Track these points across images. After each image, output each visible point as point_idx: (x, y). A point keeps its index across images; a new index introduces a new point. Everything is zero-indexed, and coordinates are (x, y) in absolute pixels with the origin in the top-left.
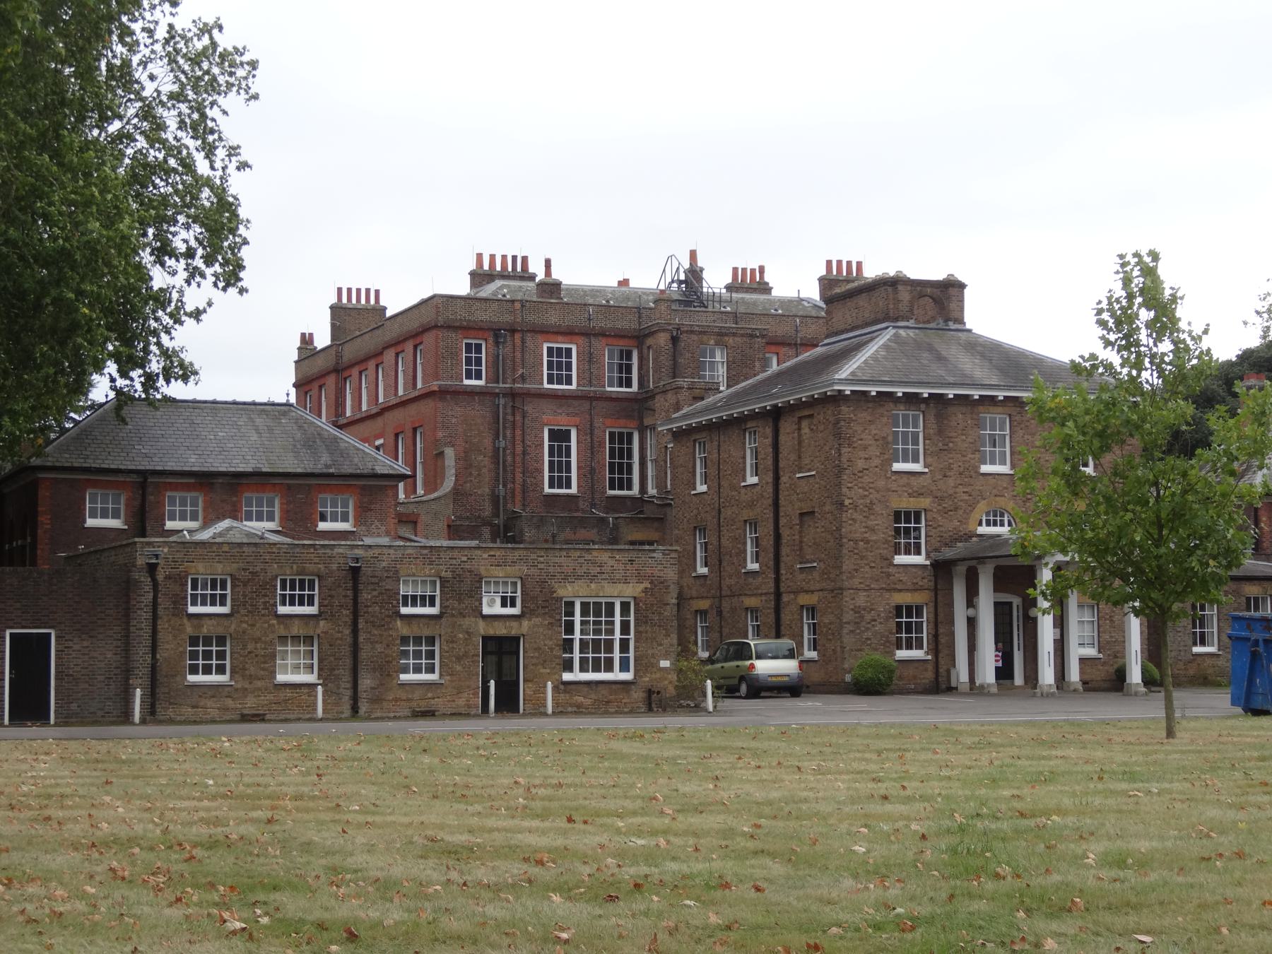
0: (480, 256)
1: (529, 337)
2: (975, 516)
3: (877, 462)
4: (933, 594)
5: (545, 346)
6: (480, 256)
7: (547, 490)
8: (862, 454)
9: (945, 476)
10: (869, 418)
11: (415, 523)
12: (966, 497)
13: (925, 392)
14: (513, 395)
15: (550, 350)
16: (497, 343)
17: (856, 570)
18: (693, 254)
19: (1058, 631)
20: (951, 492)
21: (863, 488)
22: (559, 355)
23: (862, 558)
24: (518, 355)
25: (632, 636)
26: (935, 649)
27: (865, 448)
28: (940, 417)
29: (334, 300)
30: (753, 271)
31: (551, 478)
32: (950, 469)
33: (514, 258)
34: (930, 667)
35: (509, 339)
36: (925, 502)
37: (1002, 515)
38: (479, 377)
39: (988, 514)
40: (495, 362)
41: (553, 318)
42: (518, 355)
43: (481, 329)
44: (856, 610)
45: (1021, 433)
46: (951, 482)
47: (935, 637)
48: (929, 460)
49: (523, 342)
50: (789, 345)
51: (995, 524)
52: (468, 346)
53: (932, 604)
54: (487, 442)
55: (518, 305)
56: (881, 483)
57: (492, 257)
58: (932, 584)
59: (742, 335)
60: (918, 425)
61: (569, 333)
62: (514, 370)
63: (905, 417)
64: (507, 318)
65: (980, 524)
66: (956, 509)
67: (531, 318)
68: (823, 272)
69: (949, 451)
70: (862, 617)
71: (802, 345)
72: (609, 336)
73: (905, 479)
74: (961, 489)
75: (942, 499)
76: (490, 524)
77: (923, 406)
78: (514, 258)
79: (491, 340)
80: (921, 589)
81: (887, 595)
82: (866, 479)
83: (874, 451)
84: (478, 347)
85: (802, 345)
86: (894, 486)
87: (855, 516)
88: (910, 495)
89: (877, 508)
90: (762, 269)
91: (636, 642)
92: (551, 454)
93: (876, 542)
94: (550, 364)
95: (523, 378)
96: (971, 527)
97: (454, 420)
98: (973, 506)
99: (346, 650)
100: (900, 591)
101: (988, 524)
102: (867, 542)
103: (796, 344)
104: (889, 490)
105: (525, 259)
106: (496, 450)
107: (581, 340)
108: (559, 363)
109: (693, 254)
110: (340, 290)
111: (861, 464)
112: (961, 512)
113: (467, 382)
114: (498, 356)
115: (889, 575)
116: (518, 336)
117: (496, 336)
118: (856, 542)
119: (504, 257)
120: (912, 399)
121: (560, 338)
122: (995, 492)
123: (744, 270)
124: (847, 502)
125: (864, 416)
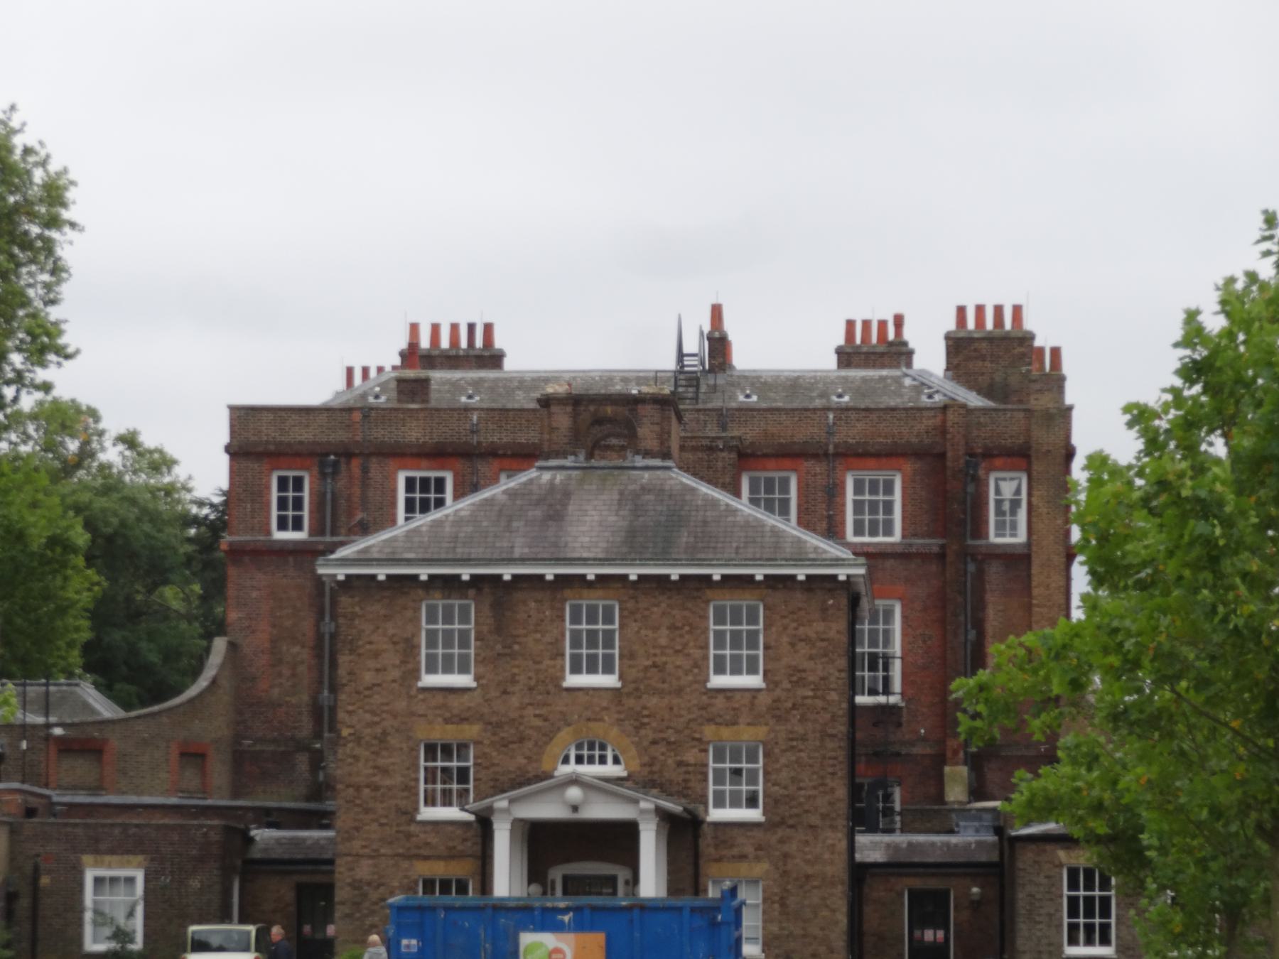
0: (414, 328)
1: (374, 464)
2: (555, 748)
3: (396, 674)
4: (479, 863)
6: (414, 328)
8: (371, 664)
9: (505, 692)
10: (383, 612)
12: (538, 722)
13: (466, 573)
15: (410, 483)
16: (323, 475)
17: (357, 829)
18: (717, 312)
20: (513, 715)
21: (373, 713)
23: (367, 811)
25: (1113, 921)
27: (377, 655)
28: (499, 608)
30: (882, 325)
32: (513, 680)
33: (471, 327)
35: (343, 467)
36: (472, 731)
37: (603, 747)
38: (298, 526)
39: (579, 747)
41: (414, 433)
42: (357, 491)
43: (298, 454)
44: (356, 885)
45: (634, 626)
46: (515, 701)
48: (482, 670)
49: (365, 471)
50: (815, 456)
51: (591, 760)
52: (283, 483)
53: (478, 878)
54: (307, 626)
55: (357, 416)
56: (401, 705)
57: (435, 329)
58: (478, 848)
59: (695, 449)
60: (467, 619)
62: (350, 514)
64: (341, 436)
65: (566, 760)
66: (522, 740)
67: (381, 434)
68: (951, 325)
69: (513, 656)
70: (365, 895)
71: (836, 455)
72: (505, 456)
73: (439, 699)
74: (530, 711)
75: (499, 725)
76: (307, 749)
77: (472, 592)
78: (471, 327)
79: (316, 470)
80: (460, 856)
81: (405, 864)
82: (377, 699)
83: (391, 658)
84: (298, 483)
85: (836, 455)
86: (421, 709)
87: (357, 751)
88: (447, 721)
89: (393, 741)
90: (899, 321)
92: (887, 633)
93: (389, 788)
96: (546, 766)
97: (254, 594)
98: (549, 736)
100: (426, 858)
101: (579, 760)
102: (376, 788)
103: (826, 455)
104: (412, 714)
105: (488, 328)
106: (320, 637)
107: (460, 464)
109: (717, 312)
110: (350, 371)
111: (369, 677)
112: (530, 744)
113: (279, 535)
114: (324, 494)
115: (409, 836)
116: (356, 464)
117: (322, 465)
118: (358, 788)
119: (455, 328)
120: (449, 584)
121: (424, 463)
122: (588, 714)
123: (866, 324)
124: (345, 732)
125: (377, 608)
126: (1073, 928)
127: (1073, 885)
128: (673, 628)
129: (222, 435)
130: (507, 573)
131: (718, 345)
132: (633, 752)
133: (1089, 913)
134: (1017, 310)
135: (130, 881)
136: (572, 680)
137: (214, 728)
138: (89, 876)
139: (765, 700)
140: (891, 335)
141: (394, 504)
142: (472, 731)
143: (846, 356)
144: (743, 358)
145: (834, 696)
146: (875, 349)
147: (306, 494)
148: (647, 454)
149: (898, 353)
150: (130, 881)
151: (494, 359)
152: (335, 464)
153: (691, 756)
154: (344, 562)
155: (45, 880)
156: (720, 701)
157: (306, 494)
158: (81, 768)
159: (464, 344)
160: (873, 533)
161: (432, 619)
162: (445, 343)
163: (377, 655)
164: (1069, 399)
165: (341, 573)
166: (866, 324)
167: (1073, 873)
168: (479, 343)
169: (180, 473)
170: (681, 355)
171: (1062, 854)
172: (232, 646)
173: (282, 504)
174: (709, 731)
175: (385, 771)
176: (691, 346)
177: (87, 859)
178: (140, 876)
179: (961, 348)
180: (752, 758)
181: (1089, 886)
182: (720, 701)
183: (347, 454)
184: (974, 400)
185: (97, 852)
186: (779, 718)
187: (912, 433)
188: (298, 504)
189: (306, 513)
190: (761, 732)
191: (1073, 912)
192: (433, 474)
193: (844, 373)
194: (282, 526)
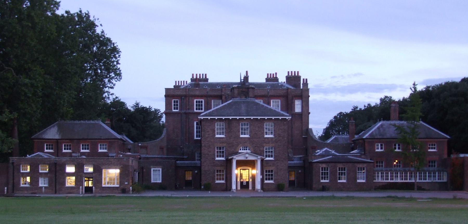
1: (190, 98)
5: (195, 100)
7: (195, 138)
8: (207, 133)
11: (147, 148)
14: (185, 113)
16: (181, 100)
18: (247, 72)
19: (261, 176)
22: (199, 103)
24: (187, 103)
26: (226, 181)
29: (175, 84)
31: (197, 135)
34: (225, 185)
38: (177, 109)
40: (181, 106)
42: (187, 103)
46: (232, 140)
47: (226, 177)
49: (189, 99)
55: (187, 90)
56: (212, 140)
61: (201, 97)
63: (220, 124)
64: (184, 93)
67: (192, 93)
68: (287, 75)
84: (177, 101)
90: (276, 74)
91: (440, 182)
92: (197, 129)
94: (197, 105)
95: (189, 109)
98: (238, 145)
99: (54, 180)
101: (243, 150)
102: (208, 154)
105: (206, 75)
108: (199, 105)
109: (247, 72)
111: (207, 136)
113: (174, 111)
116: (187, 98)
117: (181, 98)
123: (271, 74)
126: (322, 177)
127: (339, 170)
128: (258, 127)
129: (164, 93)
130: (231, 118)
131: (246, 78)
132: (252, 148)
133: (325, 175)
134: (298, 72)
135: (159, 170)
136: (241, 136)
137: (164, 144)
138: (152, 169)
139: (274, 140)
140: (275, 76)
141: (194, 105)
142: (225, 145)
143: (267, 80)
144: (251, 80)
145: (285, 139)
146: (272, 79)
147: (178, 103)
148: (251, 97)
149: (276, 79)
150: (159, 170)
151: (206, 80)
152: (184, 99)
153: (261, 149)
154: (203, 116)
155: (144, 170)
156: (266, 139)
157: (178, 103)
158: (144, 150)
159: (202, 77)
160: (199, 110)
161: (217, 126)
162: (198, 77)
163: (208, 132)
164: (309, 87)
165: (202, 118)
166: (271, 74)
167: (322, 168)
168: (204, 77)
169: (119, 98)
170: (241, 80)
171: (320, 165)
172: (167, 129)
173: (174, 105)
174: (265, 144)
175: (210, 152)
176: (242, 78)
177: (152, 166)
178: (161, 169)
179: (288, 78)
180: (272, 149)
181: (325, 170)
182: (266, 139)
183: (186, 96)
184: (290, 87)
185: (153, 165)
186: (276, 142)
187: (281, 93)
188: (177, 105)
189: (179, 107)
190: (273, 145)
191: (322, 175)
192: (201, 100)
193: (268, 83)
194: (174, 109)
